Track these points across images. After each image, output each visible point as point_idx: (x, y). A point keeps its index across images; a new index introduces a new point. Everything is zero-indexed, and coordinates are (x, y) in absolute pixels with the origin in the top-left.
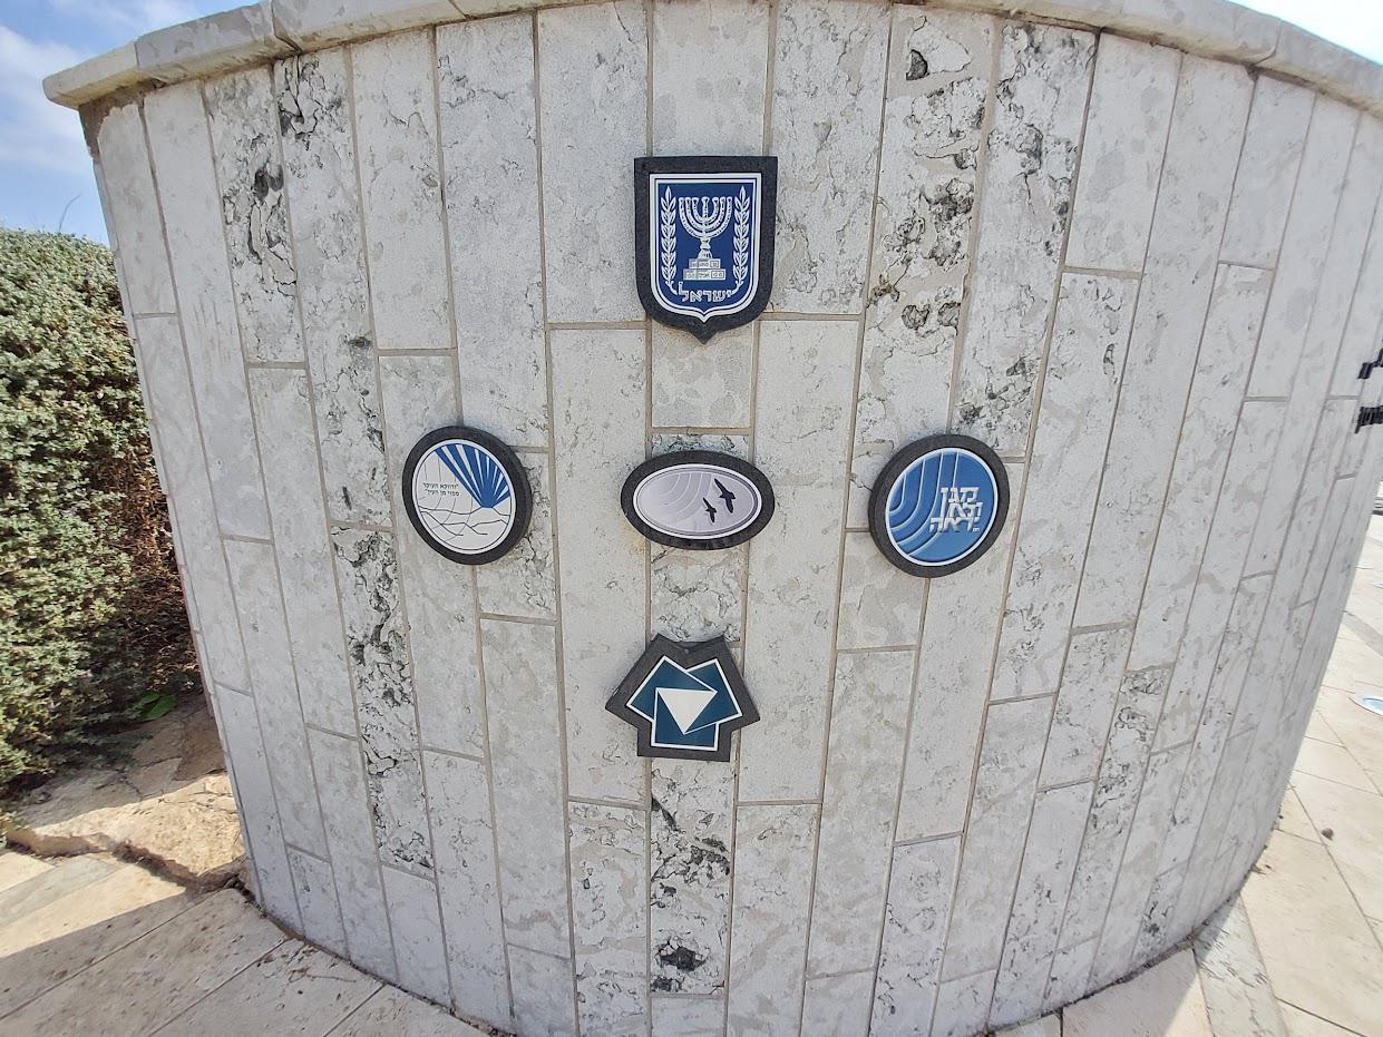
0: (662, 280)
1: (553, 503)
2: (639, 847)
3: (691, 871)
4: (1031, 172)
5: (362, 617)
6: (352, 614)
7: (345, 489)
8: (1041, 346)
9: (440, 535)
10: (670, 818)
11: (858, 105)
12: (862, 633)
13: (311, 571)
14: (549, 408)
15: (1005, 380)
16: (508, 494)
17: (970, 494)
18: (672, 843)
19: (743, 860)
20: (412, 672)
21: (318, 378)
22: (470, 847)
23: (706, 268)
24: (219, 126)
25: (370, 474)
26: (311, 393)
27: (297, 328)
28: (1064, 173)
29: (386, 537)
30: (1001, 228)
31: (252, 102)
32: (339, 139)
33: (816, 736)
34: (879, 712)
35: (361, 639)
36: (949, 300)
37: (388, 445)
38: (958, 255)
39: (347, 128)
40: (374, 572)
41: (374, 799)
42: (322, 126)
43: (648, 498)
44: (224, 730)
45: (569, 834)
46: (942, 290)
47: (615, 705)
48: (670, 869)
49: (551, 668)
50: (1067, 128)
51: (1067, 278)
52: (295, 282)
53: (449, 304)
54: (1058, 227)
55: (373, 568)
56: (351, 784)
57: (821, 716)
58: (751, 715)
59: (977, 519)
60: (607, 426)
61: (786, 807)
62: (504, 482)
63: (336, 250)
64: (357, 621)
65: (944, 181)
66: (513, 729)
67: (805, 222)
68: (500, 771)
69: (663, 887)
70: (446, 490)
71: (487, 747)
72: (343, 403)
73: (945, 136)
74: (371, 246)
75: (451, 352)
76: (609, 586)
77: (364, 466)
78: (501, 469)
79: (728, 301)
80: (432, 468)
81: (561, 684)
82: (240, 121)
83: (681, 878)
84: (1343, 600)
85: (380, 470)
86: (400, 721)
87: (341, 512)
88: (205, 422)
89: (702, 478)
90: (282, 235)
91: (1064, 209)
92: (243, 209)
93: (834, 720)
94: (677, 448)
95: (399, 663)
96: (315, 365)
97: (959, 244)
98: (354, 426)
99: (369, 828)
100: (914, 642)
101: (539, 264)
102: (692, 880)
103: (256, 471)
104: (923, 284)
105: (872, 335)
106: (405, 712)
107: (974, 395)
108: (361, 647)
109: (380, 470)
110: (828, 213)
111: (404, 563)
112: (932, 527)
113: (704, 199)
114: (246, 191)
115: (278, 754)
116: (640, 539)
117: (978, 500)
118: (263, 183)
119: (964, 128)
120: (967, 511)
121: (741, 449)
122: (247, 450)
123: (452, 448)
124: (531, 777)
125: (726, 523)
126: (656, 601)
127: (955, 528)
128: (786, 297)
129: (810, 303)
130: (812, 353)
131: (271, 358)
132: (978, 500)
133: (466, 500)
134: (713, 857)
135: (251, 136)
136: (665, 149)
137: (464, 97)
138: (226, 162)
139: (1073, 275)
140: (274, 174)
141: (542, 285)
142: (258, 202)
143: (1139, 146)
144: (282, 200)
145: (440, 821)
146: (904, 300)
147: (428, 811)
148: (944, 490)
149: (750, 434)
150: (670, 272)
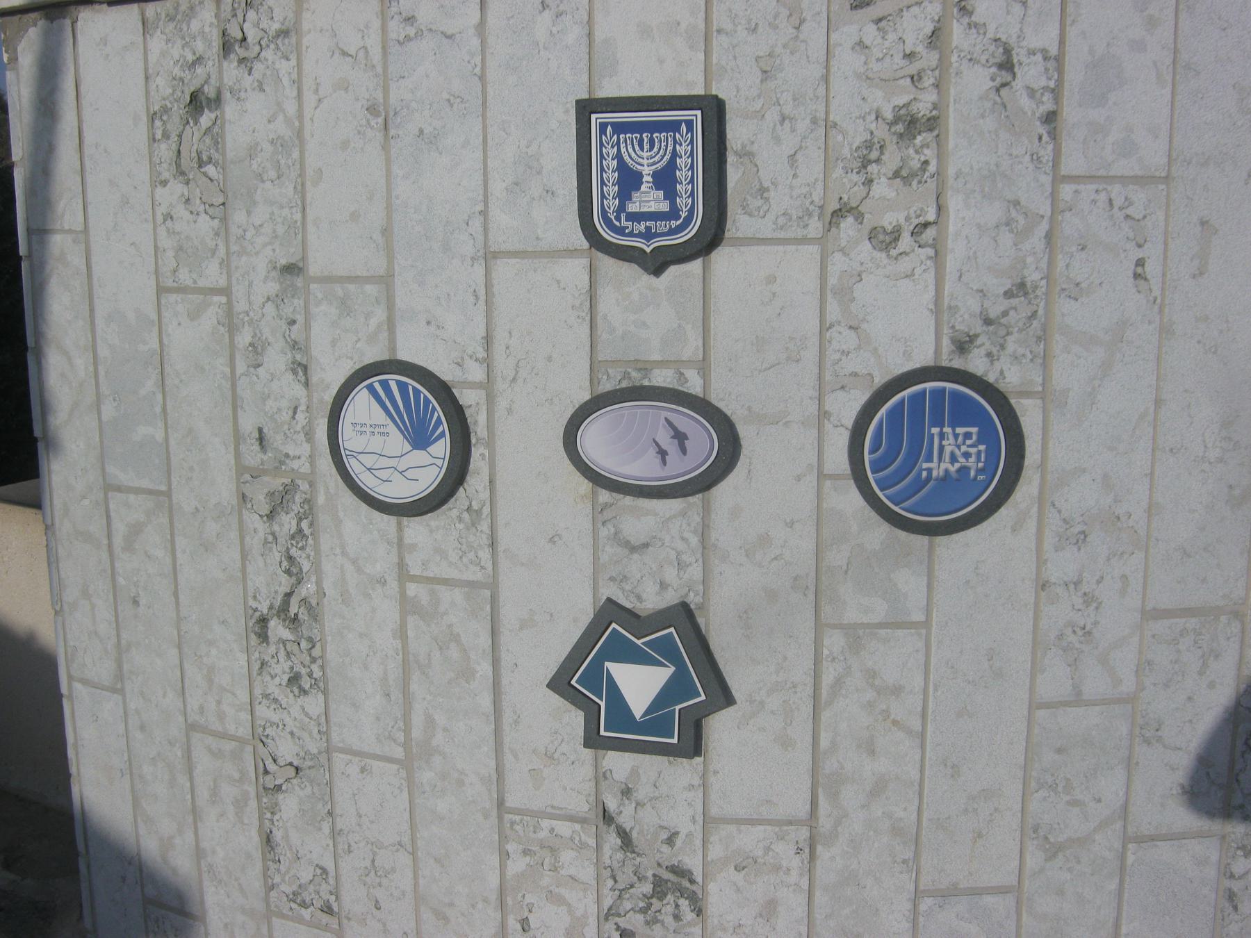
0: (604, 213)
1: (490, 444)
2: (587, 873)
3: (653, 909)
4: (1004, 85)
5: (267, 582)
6: (257, 580)
7: (260, 430)
8: (1044, 265)
9: (367, 481)
10: (625, 836)
11: (801, 37)
12: (858, 606)
13: (212, 527)
14: (488, 340)
15: (1003, 304)
16: (442, 435)
17: (968, 436)
18: (629, 870)
19: (718, 896)
20: (323, 650)
21: (240, 306)
22: (385, 881)
23: (649, 199)
24: (157, 43)
25: (290, 413)
26: (231, 323)
27: (222, 251)
28: (1043, 82)
29: (304, 486)
30: (967, 149)
31: (195, 25)
32: (285, 67)
33: (801, 731)
34: (884, 707)
35: (265, 611)
36: (922, 220)
37: (314, 379)
38: (927, 174)
39: (293, 58)
40: (287, 527)
41: (267, 823)
42: (268, 54)
43: (596, 440)
44: (76, 745)
45: (504, 856)
46: (912, 211)
47: (560, 684)
48: (627, 905)
49: (485, 641)
50: (1047, 38)
51: (1066, 191)
52: (223, 204)
53: (387, 231)
54: (1045, 138)
55: (287, 523)
56: (240, 804)
57: (807, 710)
58: (723, 696)
59: (981, 465)
60: (549, 359)
61: (769, 828)
62: (439, 422)
63: (272, 174)
64: (264, 590)
65: (901, 100)
66: (441, 720)
67: (755, 148)
68: (426, 776)
69: (618, 928)
70: (376, 431)
71: (406, 745)
72: (266, 333)
73: (898, 60)
74: (309, 172)
75: (386, 281)
76: (552, 540)
77: (284, 404)
78: (440, 411)
79: (672, 232)
80: (362, 406)
81: (496, 663)
82: (179, 43)
83: (640, 918)
84: (590, 401)
85: (302, 408)
86: (307, 715)
87: (253, 456)
88: (103, 352)
89: (652, 419)
90: (216, 156)
91: (1050, 118)
92: (174, 125)
93: (825, 716)
94: (624, 384)
95: (310, 640)
96: (239, 291)
97: (926, 162)
98: (277, 359)
99: (259, 865)
100: (922, 618)
101: (481, 192)
102: (655, 921)
103: (158, 409)
104: (890, 204)
105: (838, 263)
106: (314, 704)
107: (966, 321)
108: (263, 621)
109: (302, 408)
110: (777, 140)
111: (323, 519)
112: (924, 474)
113: (644, 135)
114: (178, 110)
115: (147, 769)
116: (585, 485)
117: (979, 442)
118: (196, 103)
119: (920, 48)
120: (967, 455)
121: (694, 385)
122: (150, 385)
123: (385, 385)
124: (461, 783)
125: (681, 467)
126: (604, 558)
127: (954, 475)
128: (739, 223)
129: (764, 227)
130: (771, 279)
131: (189, 283)
132: (979, 442)
133: (397, 442)
134: (682, 892)
135: (190, 58)
136: (608, 89)
137: (412, 35)
138: (160, 81)
139: (1074, 187)
140: (212, 95)
141: (484, 213)
142: (191, 122)
143: (1138, 46)
144: (219, 122)
145: (349, 846)
146: (869, 221)
147: (335, 834)
148: (935, 430)
149: (704, 366)
150: (612, 204)
